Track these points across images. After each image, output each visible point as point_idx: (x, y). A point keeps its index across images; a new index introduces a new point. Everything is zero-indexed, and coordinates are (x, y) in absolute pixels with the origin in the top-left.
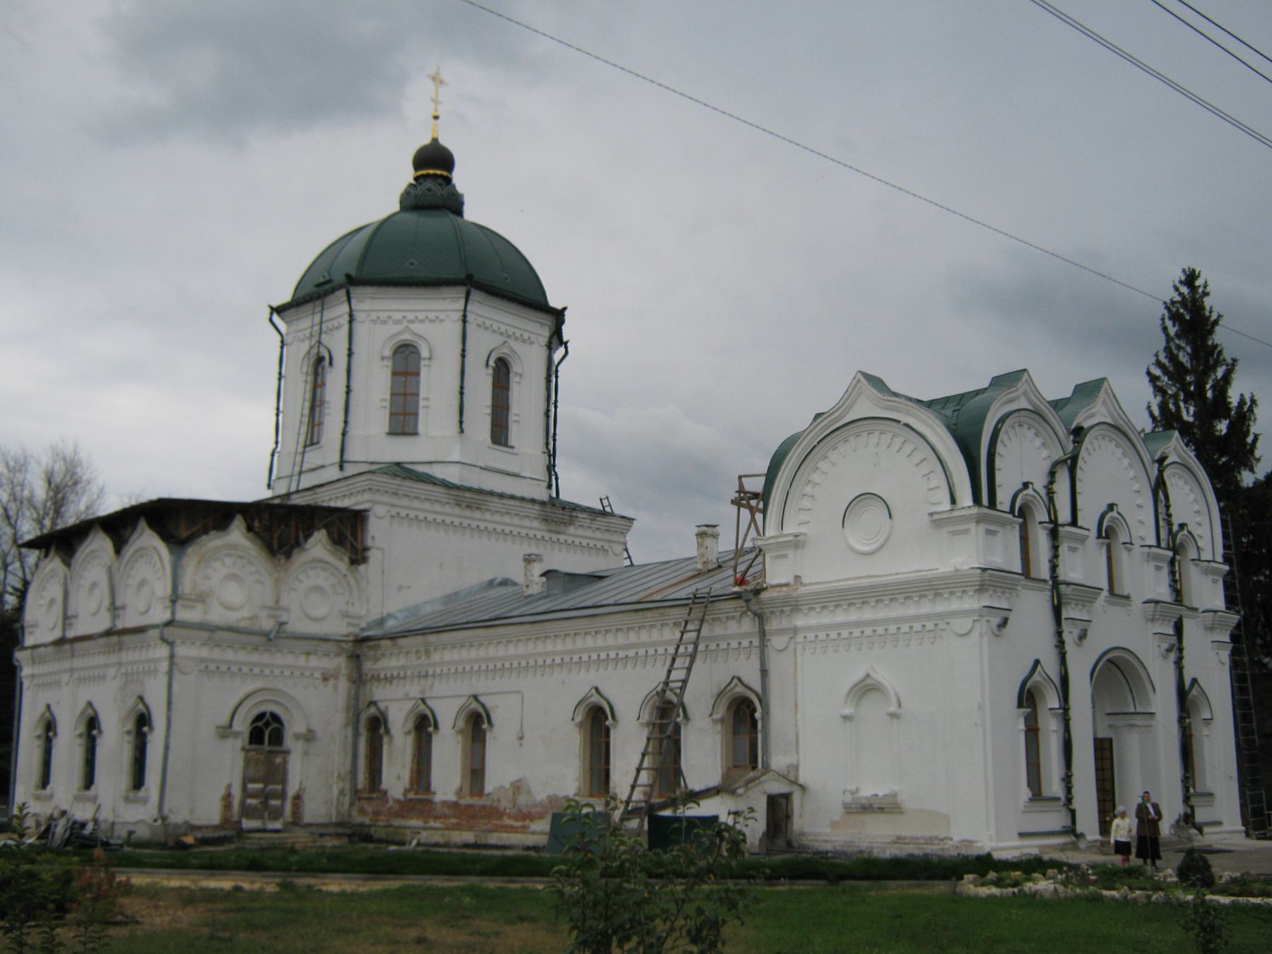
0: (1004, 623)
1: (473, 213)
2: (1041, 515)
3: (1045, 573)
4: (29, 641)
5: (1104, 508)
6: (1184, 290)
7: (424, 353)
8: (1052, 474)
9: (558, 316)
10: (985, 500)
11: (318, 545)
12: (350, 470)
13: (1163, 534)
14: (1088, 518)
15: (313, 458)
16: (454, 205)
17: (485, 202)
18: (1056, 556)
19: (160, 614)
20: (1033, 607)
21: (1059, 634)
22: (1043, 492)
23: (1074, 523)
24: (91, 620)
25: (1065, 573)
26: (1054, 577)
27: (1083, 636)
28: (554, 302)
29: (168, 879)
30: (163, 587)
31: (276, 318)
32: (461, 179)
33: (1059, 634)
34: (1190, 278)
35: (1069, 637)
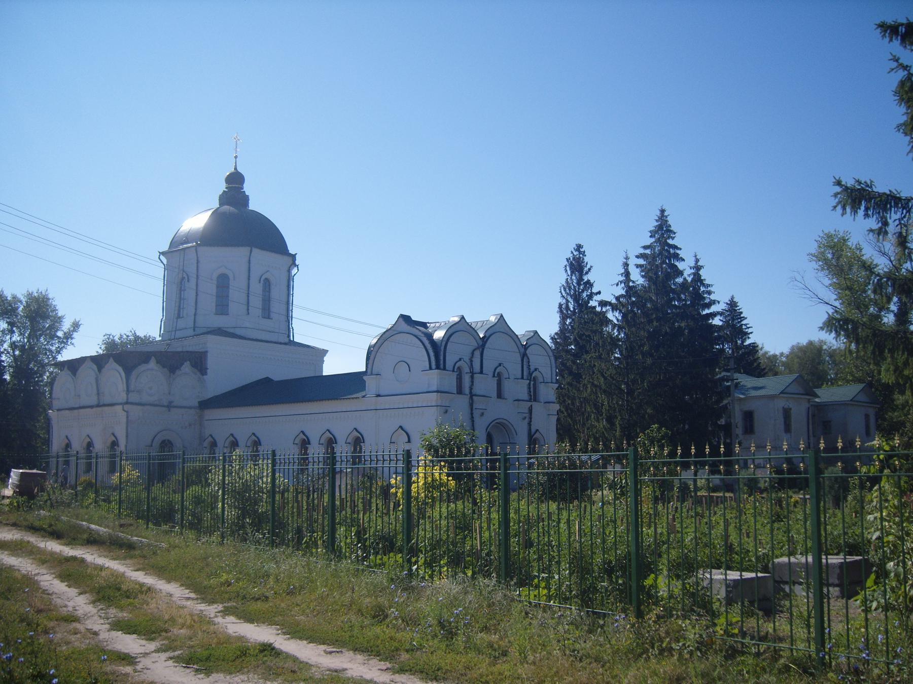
0: (446, 412)
1: (253, 206)
2: (466, 369)
3: (467, 391)
4: (56, 404)
5: (497, 364)
6: (575, 253)
7: (231, 275)
8: (473, 353)
9: (293, 257)
10: (442, 366)
11: (187, 367)
12: (198, 331)
13: (525, 373)
14: (489, 366)
15: (181, 323)
16: (245, 199)
17: (260, 202)
18: (472, 384)
19: (123, 397)
20: (462, 401)
21: (472, 414)
22: (468, 361)
23: (481, 372)
24: (378, 562)
25: (477, 390)
26: (471, 393)
27: (482, 414)
28: (292, 251)
29: (822, 342)
30: (122, 386)
31: (162, 257)
32: (248, 188)
33: (472, 414)
34: (579, 247)
35: (476, 414)
